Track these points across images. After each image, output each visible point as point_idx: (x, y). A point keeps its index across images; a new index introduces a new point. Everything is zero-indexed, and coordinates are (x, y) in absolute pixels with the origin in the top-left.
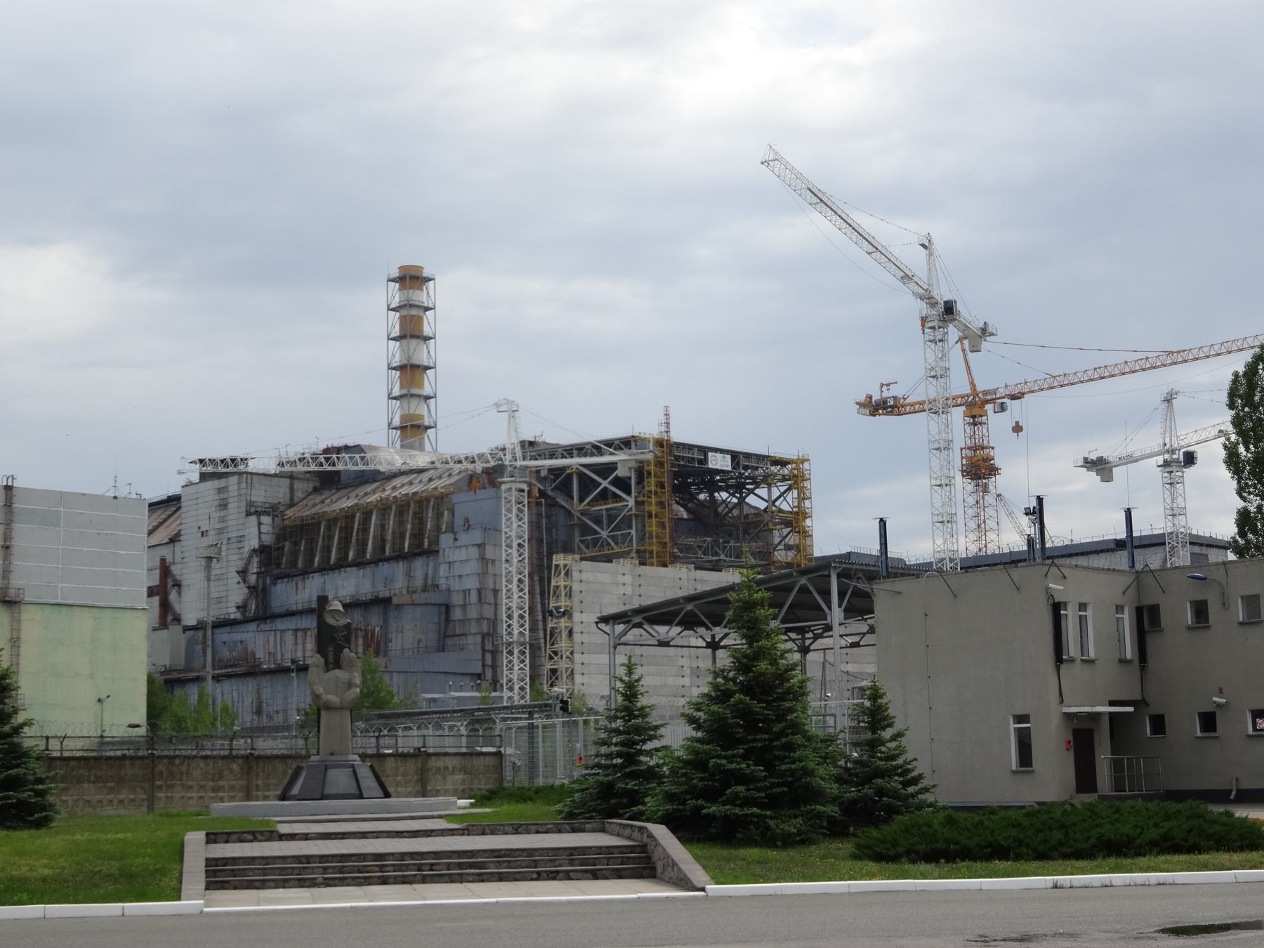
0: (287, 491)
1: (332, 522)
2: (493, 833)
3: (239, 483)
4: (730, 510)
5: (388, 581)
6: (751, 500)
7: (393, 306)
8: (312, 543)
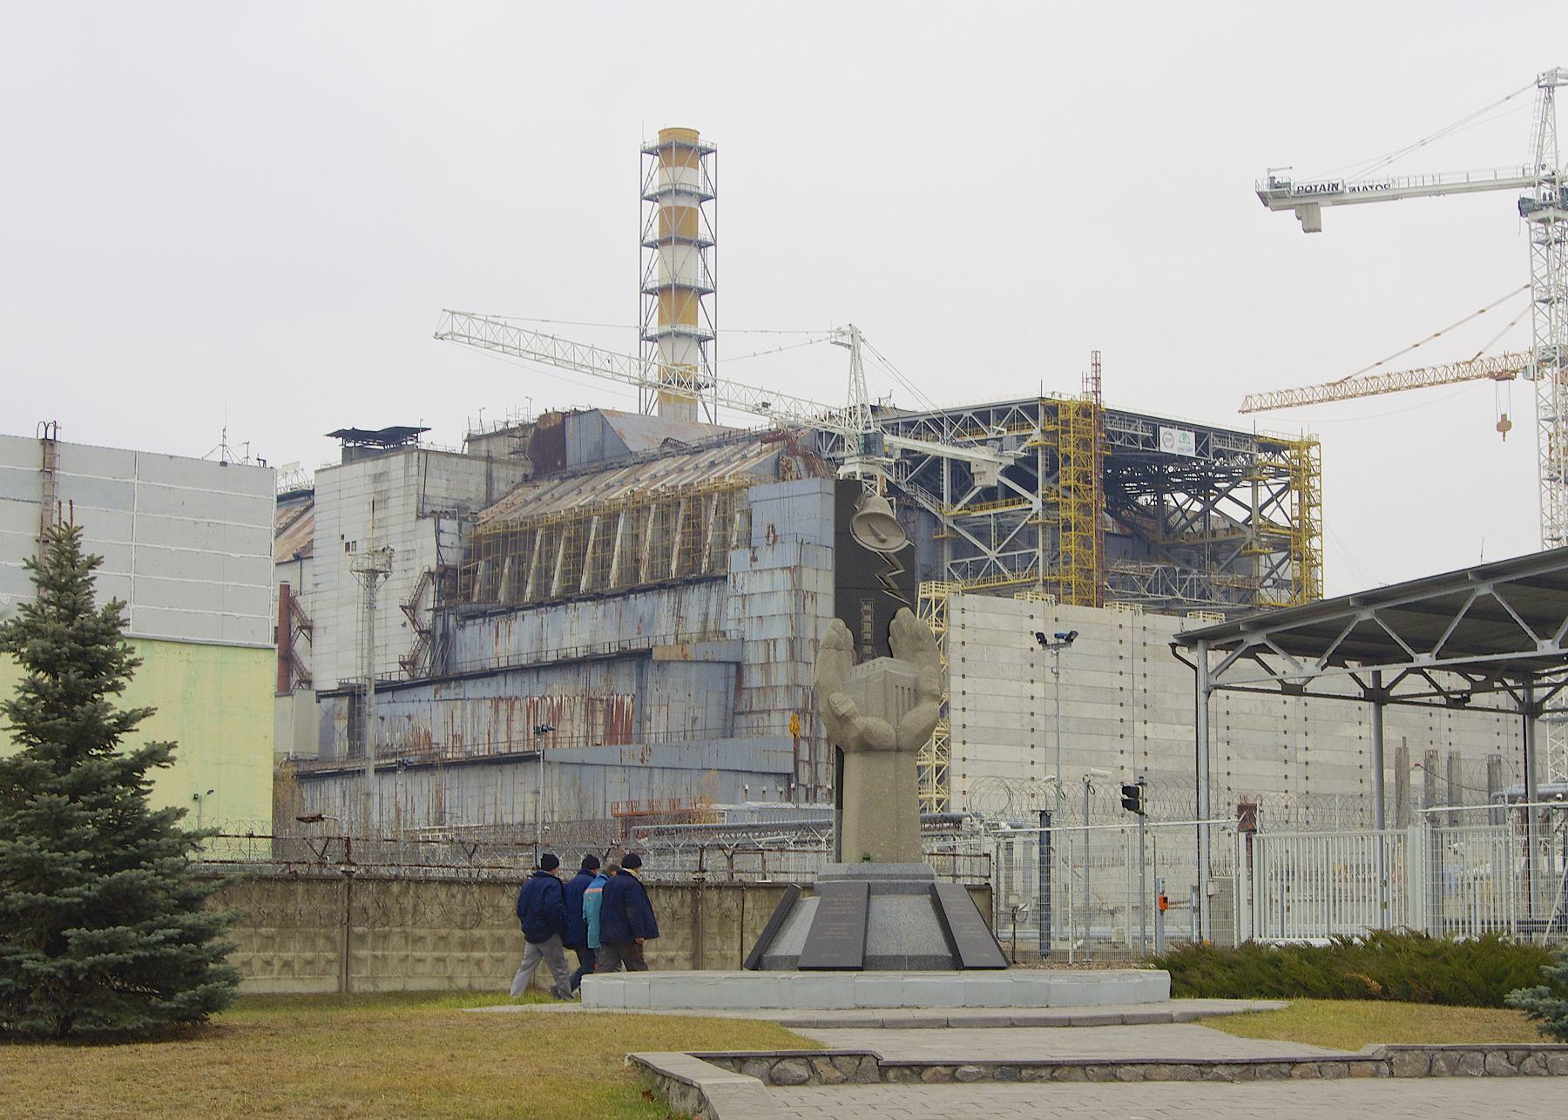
0: (483, 480)
1: (553, 531)
2: (1454, 1071)
3: (406, 468)
4: (1190, 523)
5: (642, 625)
6: (1224, 505)
7: (650, 192)
8: (520, 561)
